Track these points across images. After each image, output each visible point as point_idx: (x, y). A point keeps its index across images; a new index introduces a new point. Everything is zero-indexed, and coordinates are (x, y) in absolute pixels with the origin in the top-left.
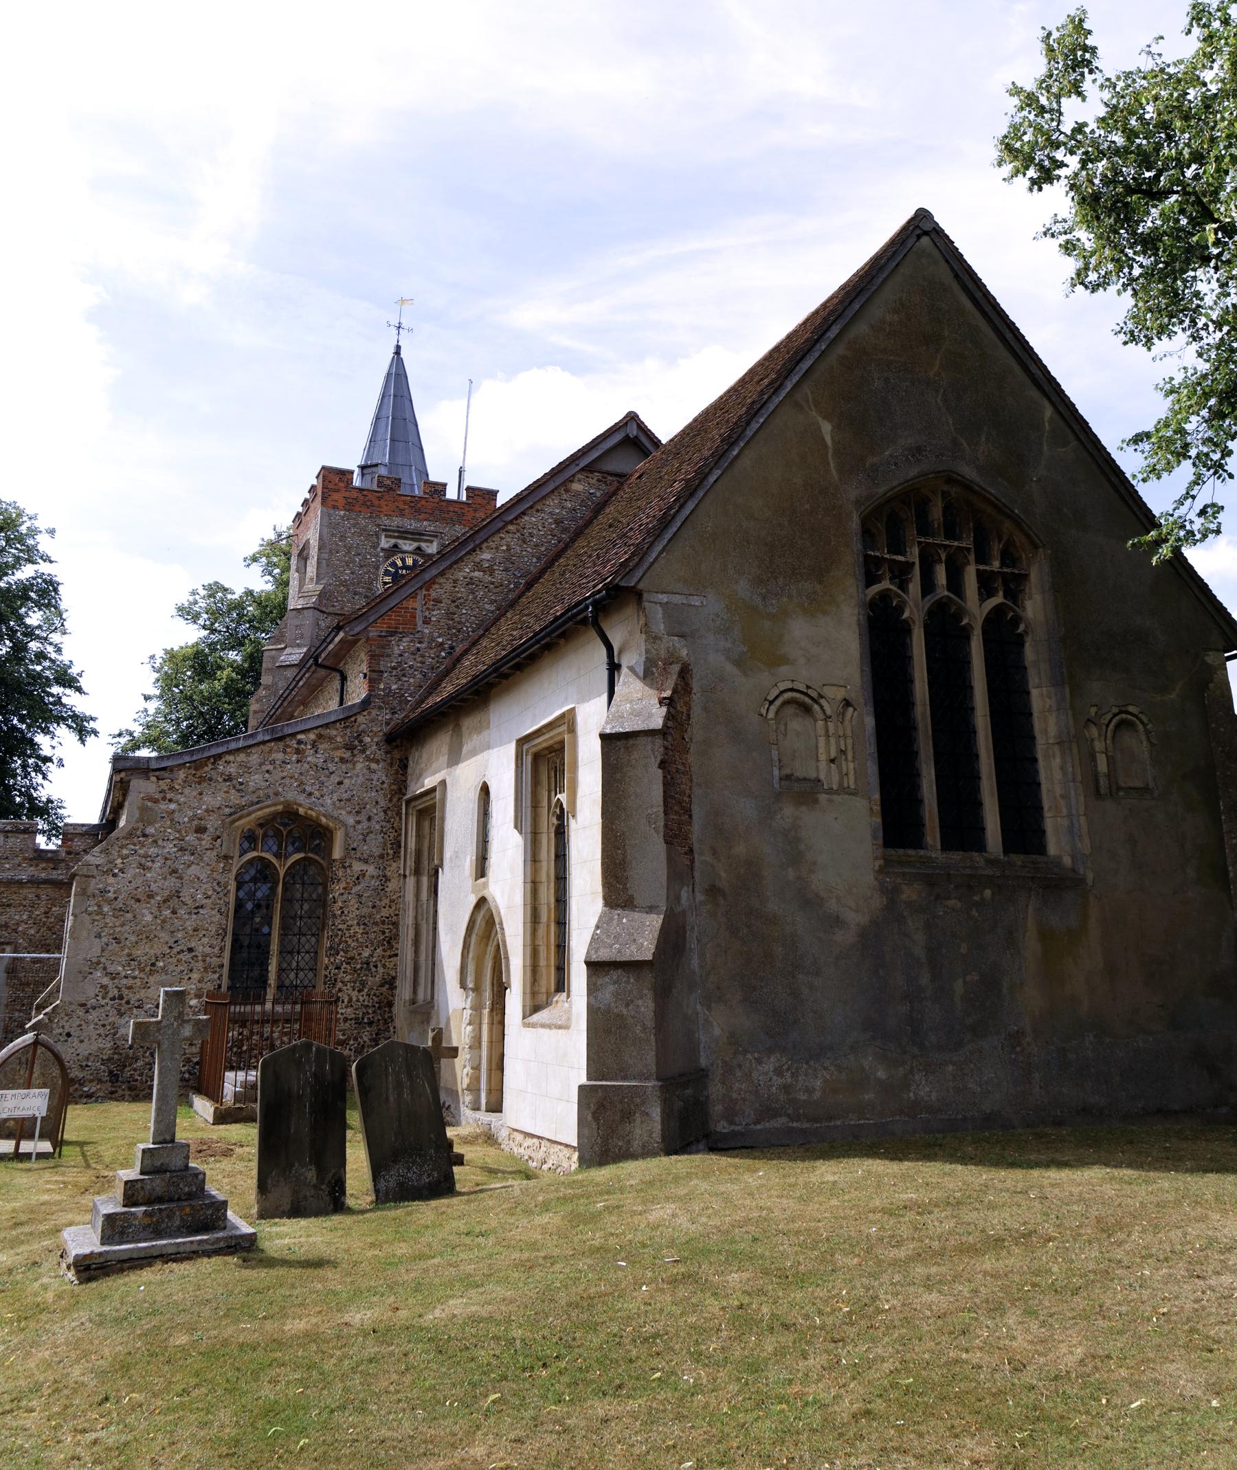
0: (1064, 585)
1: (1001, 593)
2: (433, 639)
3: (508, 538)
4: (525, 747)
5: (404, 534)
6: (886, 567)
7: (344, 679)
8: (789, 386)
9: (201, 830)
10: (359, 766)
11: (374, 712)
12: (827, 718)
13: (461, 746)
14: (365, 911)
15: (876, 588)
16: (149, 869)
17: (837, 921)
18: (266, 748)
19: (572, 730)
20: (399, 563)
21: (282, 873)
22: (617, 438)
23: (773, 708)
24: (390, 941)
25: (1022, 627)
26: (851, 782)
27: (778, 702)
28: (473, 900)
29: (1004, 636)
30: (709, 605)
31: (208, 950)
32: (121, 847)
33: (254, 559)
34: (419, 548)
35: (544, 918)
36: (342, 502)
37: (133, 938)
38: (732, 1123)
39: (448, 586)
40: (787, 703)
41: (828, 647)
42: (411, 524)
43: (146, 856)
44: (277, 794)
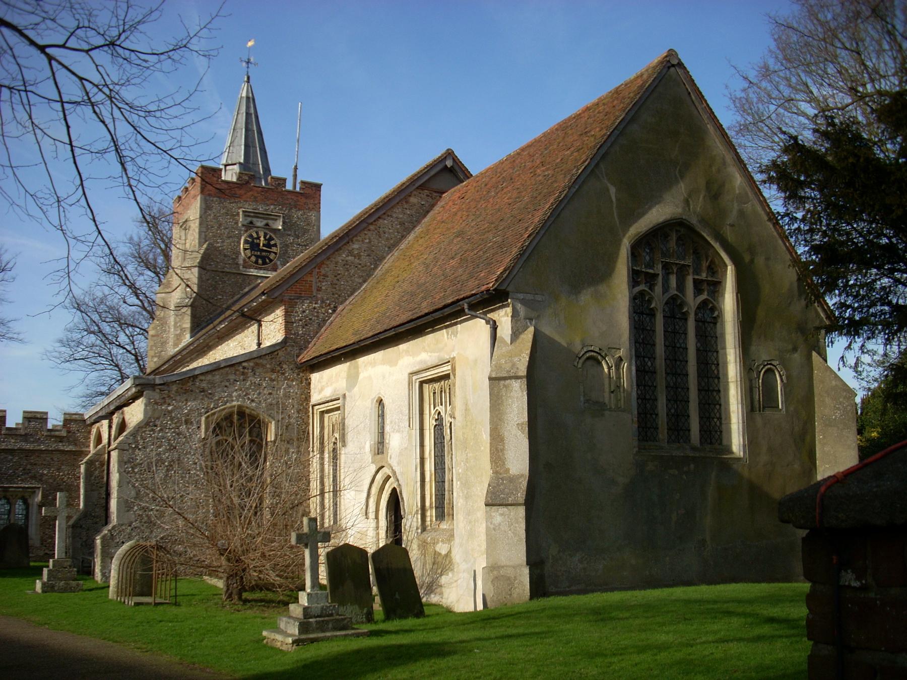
1: (706, 293)
3: (369, 233)
4: (414, 378)
6: (643, 276)
7: (260, 326)
15: (637, 289)
22: (440, 167)
23: (581, 361)
34: (267, 225)
39: (332, 266)
40: (588, 358)
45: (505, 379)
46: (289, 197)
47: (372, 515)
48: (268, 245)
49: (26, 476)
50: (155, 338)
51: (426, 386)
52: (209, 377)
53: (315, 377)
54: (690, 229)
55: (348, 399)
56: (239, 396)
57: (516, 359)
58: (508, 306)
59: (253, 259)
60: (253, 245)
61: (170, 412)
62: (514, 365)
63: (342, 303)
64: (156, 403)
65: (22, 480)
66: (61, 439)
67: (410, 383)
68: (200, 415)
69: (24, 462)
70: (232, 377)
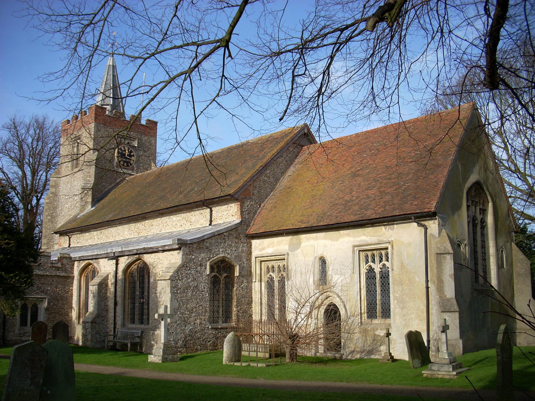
4: (356, 248)
43: (187, 274)
45: (444, 254)
46: (141, 128)
48: (130, 156)
49: (39, 291)
50: (49, 205)
51: (361, 253)
52: (210, 240)
53: (255, 243)
55: (290, 256)
56: (223, 251)
57: (445, 245)
58: (436, 219)
59: (122, 163)
60: (122, 155)
61: (193, 259)
62: (445, 248)
63: (263, 202)
64: (187, 254)
65: (36, 293)
66: (58, 269)
67: (353, 251)
68: (206, 261)
70: (219, 241)
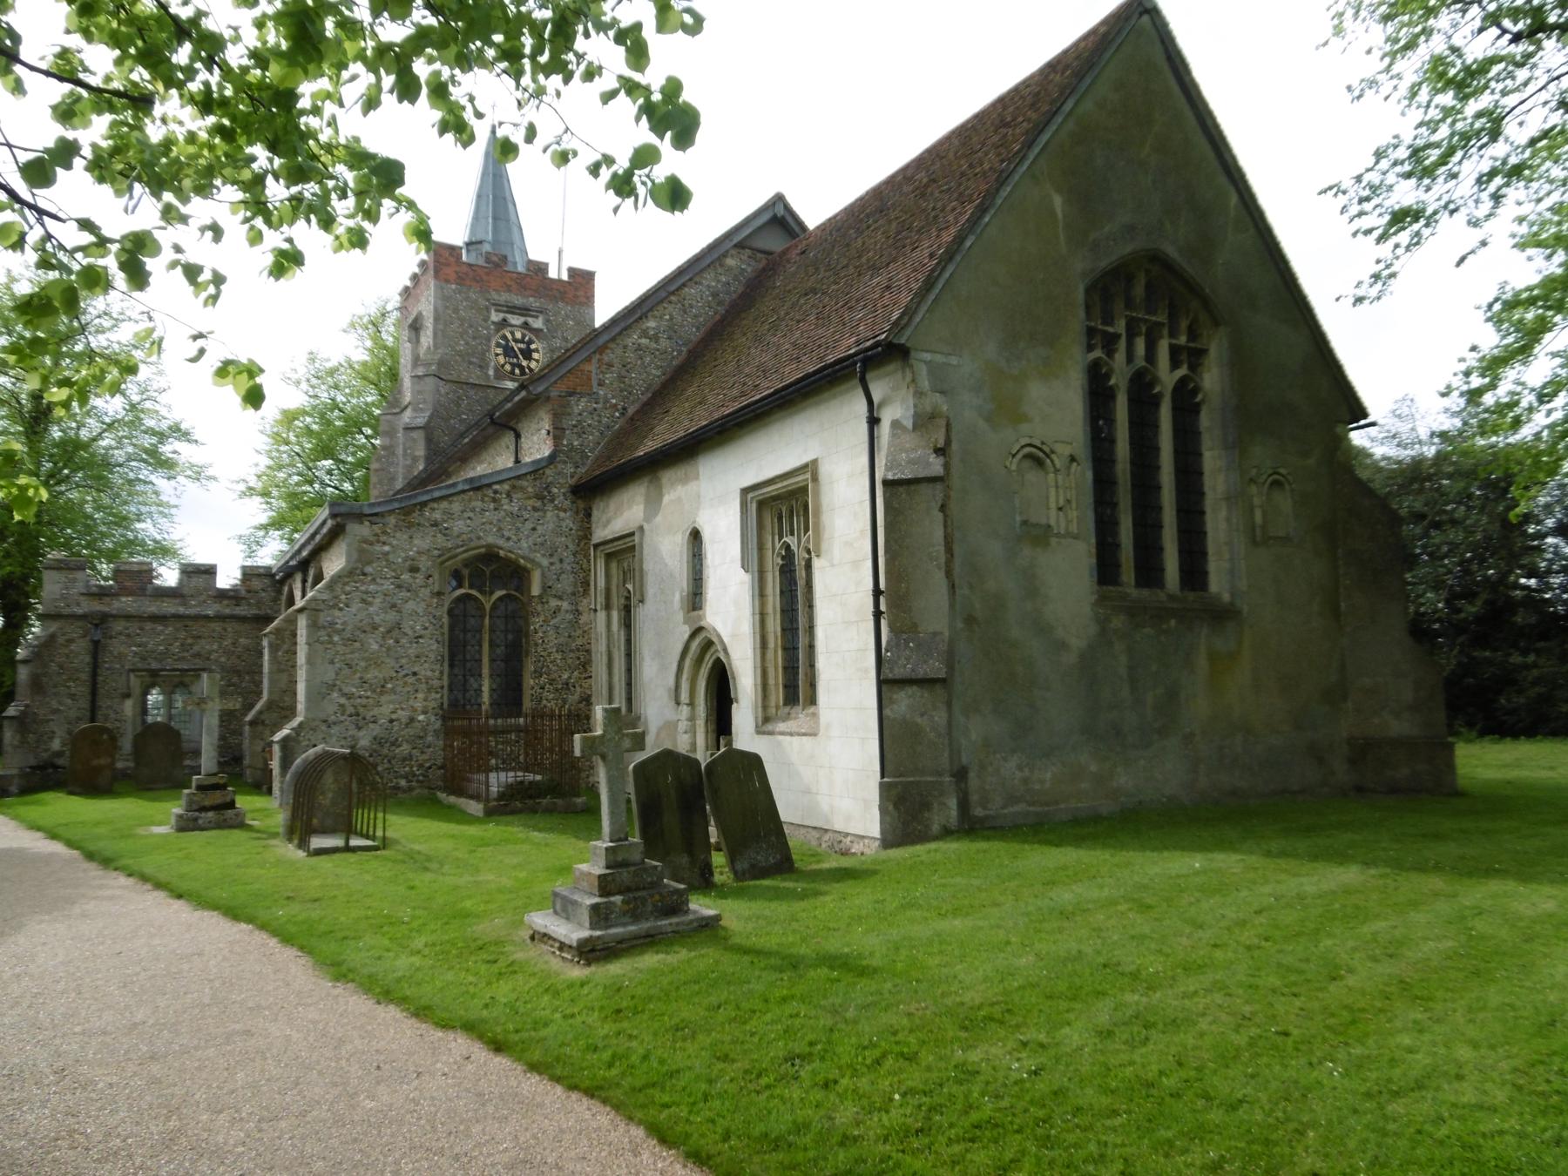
0: (1241, 364)
1: (1185, 366)
2: (607, 401)
3: (670, 308)
4: (750, 495)
5: (513, 309)
7: (518, 436)
8: (1031, 157)
9: (414, 570)
10: (549, 514)
11: (560, 466)
12: (1057, 471)
13: (660, 496)
14: (561, 640)
16: (370, 604)
17: (1063, 646)
18: (465, 497)
19: (815, 479)
20: (509, 336)
21: (488, 607)
24: (585, 665)
25: (1199, 398)
26: (1074, 528)
27: (1019, 456)
28: (686, 632)
29: (1187, 401)
30: (965, 366)
31: (429, 673)
32: (345, 584)
33: (1336, 189)
35: (771, 645)
36: (453, 276)
37: (363, 664)
38: (985, 808)
39: (619, 351)
40: (1027, 456)
41: (1057, 410)
42: (518, 301)
43: (367, 592)
44: (479, 538)
47: (684, 697)
52: (444, 504)
54: (1167, 266)
55: (647, 532)
69: (182, 635)
